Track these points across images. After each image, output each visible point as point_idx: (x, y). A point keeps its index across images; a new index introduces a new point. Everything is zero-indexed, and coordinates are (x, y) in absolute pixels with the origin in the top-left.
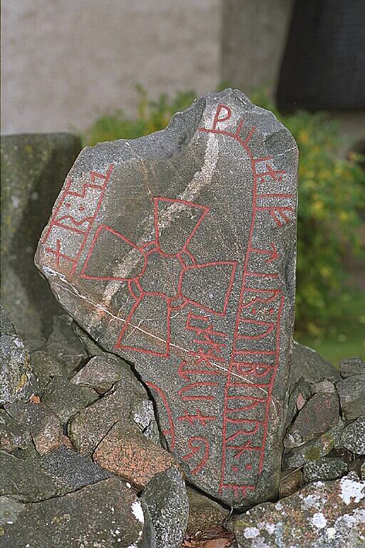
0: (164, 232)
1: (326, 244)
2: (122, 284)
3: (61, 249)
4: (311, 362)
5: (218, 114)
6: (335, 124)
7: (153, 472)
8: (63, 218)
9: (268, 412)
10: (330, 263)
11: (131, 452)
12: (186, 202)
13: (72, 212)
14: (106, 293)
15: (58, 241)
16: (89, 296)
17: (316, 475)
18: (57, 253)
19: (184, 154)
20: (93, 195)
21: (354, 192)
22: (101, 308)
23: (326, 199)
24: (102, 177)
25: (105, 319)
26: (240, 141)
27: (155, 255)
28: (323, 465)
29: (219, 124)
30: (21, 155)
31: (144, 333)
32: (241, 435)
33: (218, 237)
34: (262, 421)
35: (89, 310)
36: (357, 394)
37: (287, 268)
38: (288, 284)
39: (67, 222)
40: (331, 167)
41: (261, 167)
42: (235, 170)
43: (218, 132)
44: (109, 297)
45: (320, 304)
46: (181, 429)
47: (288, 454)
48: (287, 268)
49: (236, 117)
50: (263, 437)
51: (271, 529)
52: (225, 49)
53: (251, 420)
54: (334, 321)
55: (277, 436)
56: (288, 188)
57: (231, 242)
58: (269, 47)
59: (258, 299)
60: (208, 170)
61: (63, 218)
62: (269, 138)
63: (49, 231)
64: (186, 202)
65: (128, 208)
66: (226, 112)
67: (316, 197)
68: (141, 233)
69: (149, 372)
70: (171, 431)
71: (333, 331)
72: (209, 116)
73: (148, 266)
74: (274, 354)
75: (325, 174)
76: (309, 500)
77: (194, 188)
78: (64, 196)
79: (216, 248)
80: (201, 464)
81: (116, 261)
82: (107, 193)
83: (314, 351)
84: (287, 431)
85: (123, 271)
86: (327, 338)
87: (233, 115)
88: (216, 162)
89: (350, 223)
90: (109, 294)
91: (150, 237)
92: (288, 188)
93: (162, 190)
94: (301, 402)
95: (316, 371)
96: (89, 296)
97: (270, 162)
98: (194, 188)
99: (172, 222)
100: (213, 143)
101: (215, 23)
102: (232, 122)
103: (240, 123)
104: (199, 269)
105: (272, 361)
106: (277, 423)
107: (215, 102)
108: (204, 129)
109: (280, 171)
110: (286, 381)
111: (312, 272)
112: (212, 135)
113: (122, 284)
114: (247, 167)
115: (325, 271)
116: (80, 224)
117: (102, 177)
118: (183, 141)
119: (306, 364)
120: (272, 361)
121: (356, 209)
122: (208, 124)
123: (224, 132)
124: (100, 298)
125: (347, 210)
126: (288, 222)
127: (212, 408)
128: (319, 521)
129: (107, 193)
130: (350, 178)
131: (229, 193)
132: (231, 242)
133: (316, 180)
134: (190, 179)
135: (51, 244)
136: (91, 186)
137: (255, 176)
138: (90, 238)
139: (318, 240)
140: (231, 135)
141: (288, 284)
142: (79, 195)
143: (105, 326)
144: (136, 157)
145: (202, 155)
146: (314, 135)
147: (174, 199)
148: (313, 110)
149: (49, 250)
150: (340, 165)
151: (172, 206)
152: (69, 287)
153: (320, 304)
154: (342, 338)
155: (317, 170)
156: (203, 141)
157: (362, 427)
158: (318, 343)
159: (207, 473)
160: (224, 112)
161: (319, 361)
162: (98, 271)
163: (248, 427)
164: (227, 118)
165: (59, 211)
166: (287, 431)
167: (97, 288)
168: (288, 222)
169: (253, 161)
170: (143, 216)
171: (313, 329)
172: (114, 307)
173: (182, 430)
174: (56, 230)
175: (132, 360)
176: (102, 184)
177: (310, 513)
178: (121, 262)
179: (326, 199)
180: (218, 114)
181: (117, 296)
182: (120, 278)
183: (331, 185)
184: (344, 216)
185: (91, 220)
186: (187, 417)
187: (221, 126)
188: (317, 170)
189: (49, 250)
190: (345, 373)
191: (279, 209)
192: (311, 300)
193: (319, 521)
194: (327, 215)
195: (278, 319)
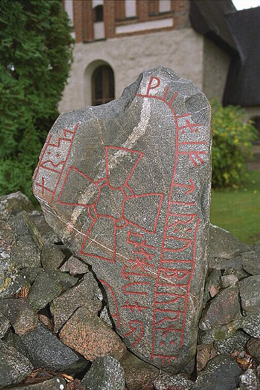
0: (112, 171)
1: (240, 153)
2: (84, 209)
3: (45, 183)
4: (225, 240)
5: (150, 84)
6: (243, 110)
7: (99, 352)
8: (45, 162)
9: (187, 304)
10: (241, 162)
11: (85, 334)
12: (127, 150)
13: (51, 158)
14: (73, 215)
15: (43, 178)
16: (63, 216)
17: (223, 346)
18: (42, 186)
19: (126, 115)
20: (65, 145)
21: (250, 135)
22: (70, 226)
23: (240, 138)
24: (71, 132)
25: (73, 233)
26: (167, 103)
27: (105, 188)
28: (228, 340)
29: (151, 90)
32: (166, 322)
33: (151, 175)
34: (183, 311)
35: (62, 226)
36: (254, 300)
37: (203, 196)
38: (203, 209)
39: (48, 165)
40: (242, 126)
41: (182, 122)
42: (162, 124)
43: (151, 96)
44: (76, 218)
45: (237, 177)
46: (124, 314)
47: (202, 333)
48: (203, 196)
49: (163, 85)
50: (184, 322)
53: (174, 311)
54: (242, 182)
55: (194, 322)
56: (203, 137)
58: (220, 85)
59: (180, 222)
60: (143, 126)
61: (45, 162)
62: (188, 100)
63: (37, 171)
64: (127, 150)
65: (88, 154)
66: (157, 81)
67: (236, 137)
68: (97, 172)
70: (118, 315)
71: (242, 187)
72: (145, 85)
73: (101, 196)
74: (192, 262)
75: (239, 128)
77: (133, 139)
78: (47, 147)
79: (149, 184)
80: (138, 340)
81: (80, 192)
82: (74, 144)
83: (227, 232)
84: (201, 318)
85: (84, 200)
86: (240, 190)
87: (161, 83)
88: (149, 119)
89: (249, 147)
90: (75, 217)
91: (103, 175)
92: (203, 137)
93: (111, 140)
94: (213, 291)
95: (228, 246)
96: (63, 216)
97: (189, 118)
98: (133, 139)
99: (118, 164)
100: (146, 104)
101: (200, 77)
102: (161, 89)
103: (167, 89)
104: (136, 199)
105: (190, 268)
106: (194, 312)
107: (149, 75)
108: (140, 95)
109: (197, 124)
110: (201, 281)
111: (234, 165)
112: (146, 99)
113: (84, 209)
114: (173, 122)
115: (239, 165)
116: (57, 166)
117: (71, 132)
118: (127, 106)
119: (222, 242)
120: (190, 268)
121: (251, 141)
122: (143, 91)
123: (155, 97)
124: (69, 218)
125: (248, 142)
126: (203, 162)
127: (145, 301)
129: (74, 144)
130: (249, 130)
131: (158, 142)
132: (159, 178)
133: (236, 131)
134: (130, 133)
135: (39, 181)
136: (64, 139)
137: (178, 128)
138: (64, 176)
139: (237, 153)
140: (160, 98)
141: (203, 209)
142: (56, 146)
143: (73, 238)
145: (139, 114)
146: (235, 114)
147: (119, 147)
148: (235, 104)
149: (37, 184)
150: (245, 125)
151: (118, 153)
152: (51, 210)
153: (237, 177)
154: (245, 190)
155: (236, 127)
156: (140, 104)
157: (258, 319)
158: (236, 192)
159: (143, 346)
160: (155, 82)
161: (231, 239)
163: (173, 315)
164: (157, 86)
165: (44, 158)
166: (201, 318)
167: (68, 211)
168: (203, 162)
169: (176, 118)
170: (98, 160)
171: (235, 186)
172: (78, 225)
173: (124, 315)
174: (41, 170)
175: (91, 263)
176: (71, 137)
178: (83, 193)
179: (240, 138)
180: (150, 84)
181: (80, 217)
182: (82, 205)
183: (241, 133)
184: (246, 144)
185: (64, 162)
188: (236, 127)
189: (37, 184)
190: (246, 266)
191: (195, 152)
192: (234, 176)
194: (240, 144)
195: (195, 236)
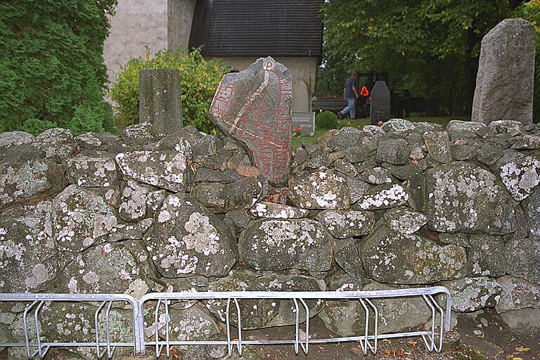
27: (249, 109)
30: (159, 76)
31: (247, 134)
41: (282, 81)
51: (301, 187)
52: (169, 30)
57: (274, 105)
60: (266, 83)
69: (250, 146)
76: (311, 178)
77: (261, 88)
93: (252, 88)
98: (261, 88)
100: (267, 74)
122: (265, 68)
124: (233, 123)
128: (314, 184)
144: (69, 73)
162: (232, 114)
177: (312, 181)
186: (262, 158)
187: (269, 69)
193: (314, 184)
